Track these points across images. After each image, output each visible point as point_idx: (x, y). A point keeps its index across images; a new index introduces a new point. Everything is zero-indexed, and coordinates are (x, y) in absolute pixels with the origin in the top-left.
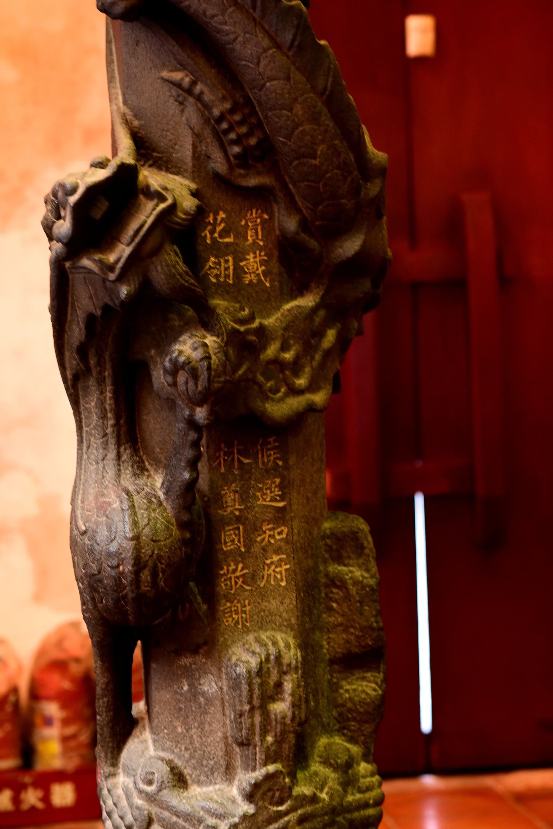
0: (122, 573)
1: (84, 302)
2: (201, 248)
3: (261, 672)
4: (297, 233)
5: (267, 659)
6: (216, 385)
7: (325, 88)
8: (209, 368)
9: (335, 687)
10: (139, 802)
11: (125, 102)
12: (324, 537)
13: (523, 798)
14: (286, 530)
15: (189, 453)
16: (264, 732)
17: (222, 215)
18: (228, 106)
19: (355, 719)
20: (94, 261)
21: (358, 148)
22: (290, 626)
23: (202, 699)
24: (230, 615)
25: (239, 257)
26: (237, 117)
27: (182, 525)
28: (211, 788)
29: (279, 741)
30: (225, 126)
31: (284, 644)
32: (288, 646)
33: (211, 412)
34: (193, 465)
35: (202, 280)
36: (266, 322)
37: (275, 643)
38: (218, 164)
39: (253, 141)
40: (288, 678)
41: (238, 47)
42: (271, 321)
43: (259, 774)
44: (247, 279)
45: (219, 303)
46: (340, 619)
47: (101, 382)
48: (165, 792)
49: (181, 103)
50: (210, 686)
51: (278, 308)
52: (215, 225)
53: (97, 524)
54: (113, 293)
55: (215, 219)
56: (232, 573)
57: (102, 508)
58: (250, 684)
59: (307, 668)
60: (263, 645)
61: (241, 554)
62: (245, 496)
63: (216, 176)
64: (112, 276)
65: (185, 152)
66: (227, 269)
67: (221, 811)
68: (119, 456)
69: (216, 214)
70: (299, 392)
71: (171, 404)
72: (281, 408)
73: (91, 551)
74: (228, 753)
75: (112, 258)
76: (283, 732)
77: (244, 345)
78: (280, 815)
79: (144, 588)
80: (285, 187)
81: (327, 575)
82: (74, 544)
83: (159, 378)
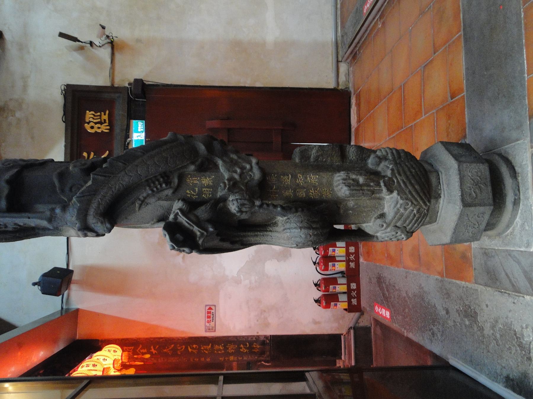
0: (313, 233)
1: (216, 242)
2: (199, 200)
3: (349, 186)
4: (195, 166)
5: (344, 183)
6: (247, 197)
7: (141, 152)
8: (240, 199)
9: (351, 161)
10: (389, 230)
11: (148, 223)
12: (301, 162)
13: (359, 121)
14: (299, 175)
15: (271, 208)
16: (369, 186)
17: (188, 191)
18: (148, 188)
19: (362, 155)
20: (199, 239)
21: (166, 143)
22: (332, 175)
23: (355, 206)
24: (327, 195)
25: (203, 186)
26: (152, 185)
27: (297, 211)
28: (386, 205)
29: (373, 181)
30: (155, 189)
31: (339, 177)
32: (339, 176)
33: (257, 199)
34: (275, 206)
35: (210, 199)
36: (226, 178)
37: (339, 181)
38: (169, 192)
39: (161, 180)
40: (351, 177)
41: (124, 183)
42: (226, 176)
43: (384, 190)
44: (211, 184)
45: (220, 194)
46: (329, 158)
47: (245, 236)
48: (386, 221)
49: (147, 204)
50: (351, 204)
51: (222, 174)
52: (191, 194)
53: (294, 241)
54: (212, 233)
55: (189, 194)
56: (313, 194)
57: (289, 239)
58: (353, 190)
59: (347, 170)
60: (339, 185)
61: (307, 191)
62: (287, 188)
63: (174, 193)
64: (205, 233)
65: (165, 203)
66: (207, 191)
67: (395, 202)
68: (271, 231)
69: (187, 193)
70: (251, 167)
71: (253, 213)
72: (257, 174)
73: (304, 244)
74: (375, 198)
75: (198, 233)
76: (370, 179)
77: (233, 186)
78: (398, 182)
79: (318, 226)
80: (179, 169)
81: (314, 162)
82: (300, 248)
83: (244, 216)
